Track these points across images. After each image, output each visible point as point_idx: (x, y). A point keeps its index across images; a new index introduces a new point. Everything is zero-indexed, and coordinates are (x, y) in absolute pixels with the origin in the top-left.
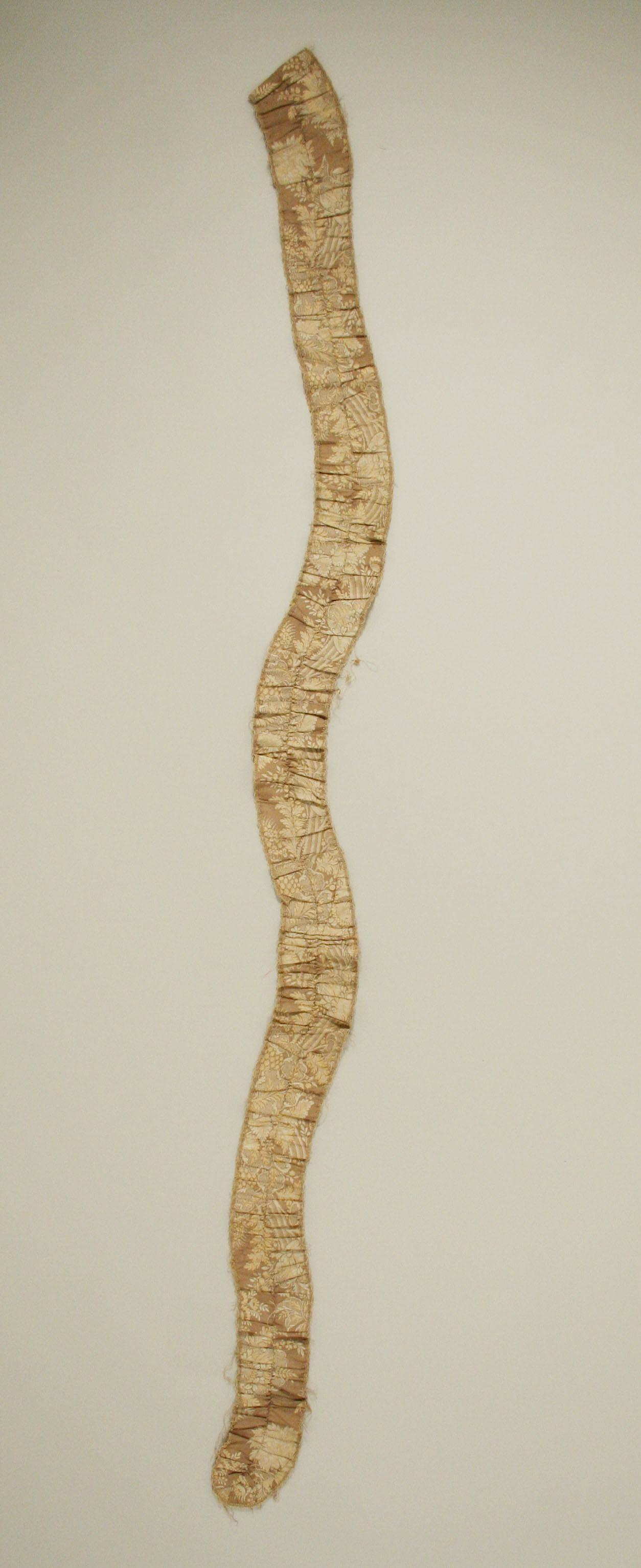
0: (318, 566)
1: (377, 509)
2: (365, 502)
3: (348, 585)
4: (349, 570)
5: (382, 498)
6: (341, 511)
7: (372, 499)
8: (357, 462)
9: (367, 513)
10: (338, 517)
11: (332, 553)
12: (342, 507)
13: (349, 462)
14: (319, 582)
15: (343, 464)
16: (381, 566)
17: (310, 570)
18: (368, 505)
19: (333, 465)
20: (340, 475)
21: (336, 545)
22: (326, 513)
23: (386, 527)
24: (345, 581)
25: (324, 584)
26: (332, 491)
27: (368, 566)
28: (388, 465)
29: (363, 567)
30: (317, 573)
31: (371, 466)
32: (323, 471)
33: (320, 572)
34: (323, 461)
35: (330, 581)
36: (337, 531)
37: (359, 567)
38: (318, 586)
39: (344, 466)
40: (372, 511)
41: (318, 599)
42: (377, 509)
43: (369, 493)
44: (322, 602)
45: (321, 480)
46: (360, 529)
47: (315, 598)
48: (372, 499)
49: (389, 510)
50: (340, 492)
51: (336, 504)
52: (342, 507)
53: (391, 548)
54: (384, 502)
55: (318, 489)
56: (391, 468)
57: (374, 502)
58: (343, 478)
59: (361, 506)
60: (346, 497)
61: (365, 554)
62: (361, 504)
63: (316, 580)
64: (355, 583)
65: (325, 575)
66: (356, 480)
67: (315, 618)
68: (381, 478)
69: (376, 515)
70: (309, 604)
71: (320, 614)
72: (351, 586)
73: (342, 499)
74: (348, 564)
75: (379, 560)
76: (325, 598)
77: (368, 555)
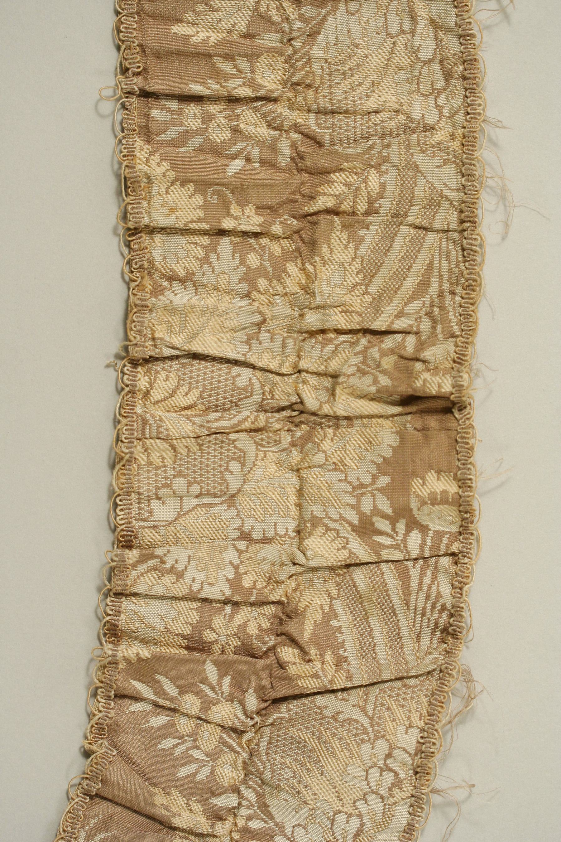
0: (177, 556)
1: (414, 251)
2: (352, 220)
3: (332, 614)
4: (322, 549)
5: (434, 203)
6: (250, 278)
7: (385, 205)
8: (313, 35)
9: (369, 273)
10: (239, 311)
11: (234, 482)
12: (253, 260)
13: (271, 40)
14: (198, 628)
15: (243, 48)
16: (465, 511)
17: (143, 580)
18: (370, 236)
19: (204, 55)
20: (233, 100)
21: (244, 441)
22: (180, 297)
23: (464, 334)
24: (314, 600)
25: (222, 630)
26: (202, 186)
27: (404, 514)
28: (452, 44)
29: (383, 525)
30: (182, 589)
31: (376, 60)
32: (155, 86)
33: (195, 578)
34: (155, 35)
35: (244, 614)
36: (244, 376)
37: (365, 529)
38: (197, 646)
39: (252, 57)
40: (392, 262)
41: (207, 704)
42: (414, 251)
43: (374, 180)
44: (224, 712)
45: (147, 133)
46: (345, 358)
47: (191, 703)
48: (385, 205)
49: (469, 253)
50: (240, 190)
51: (225, 243)
52: (253, 260)
53: (489, 420)
54: (447, 217)
55: (128, 185)
56: (469, 61)
57: (398, 217)
58: (249, 120)
59: (336, 246)
60: (269, 210)
61: (385, 466)
62: (339, 236)
63: (183, 619)
64: (357, 599)
65: (219, 590)
66: (311, 122)
67: (209, 790)
68: (421, 109)
69: (409, 284)
70: (169, 731)
71: (228, 773)
72: (343, 619)
73: (252, 220)
74: (316, 522)
75: (453, 488)
76: (236, 696)
77: (400, 469)
